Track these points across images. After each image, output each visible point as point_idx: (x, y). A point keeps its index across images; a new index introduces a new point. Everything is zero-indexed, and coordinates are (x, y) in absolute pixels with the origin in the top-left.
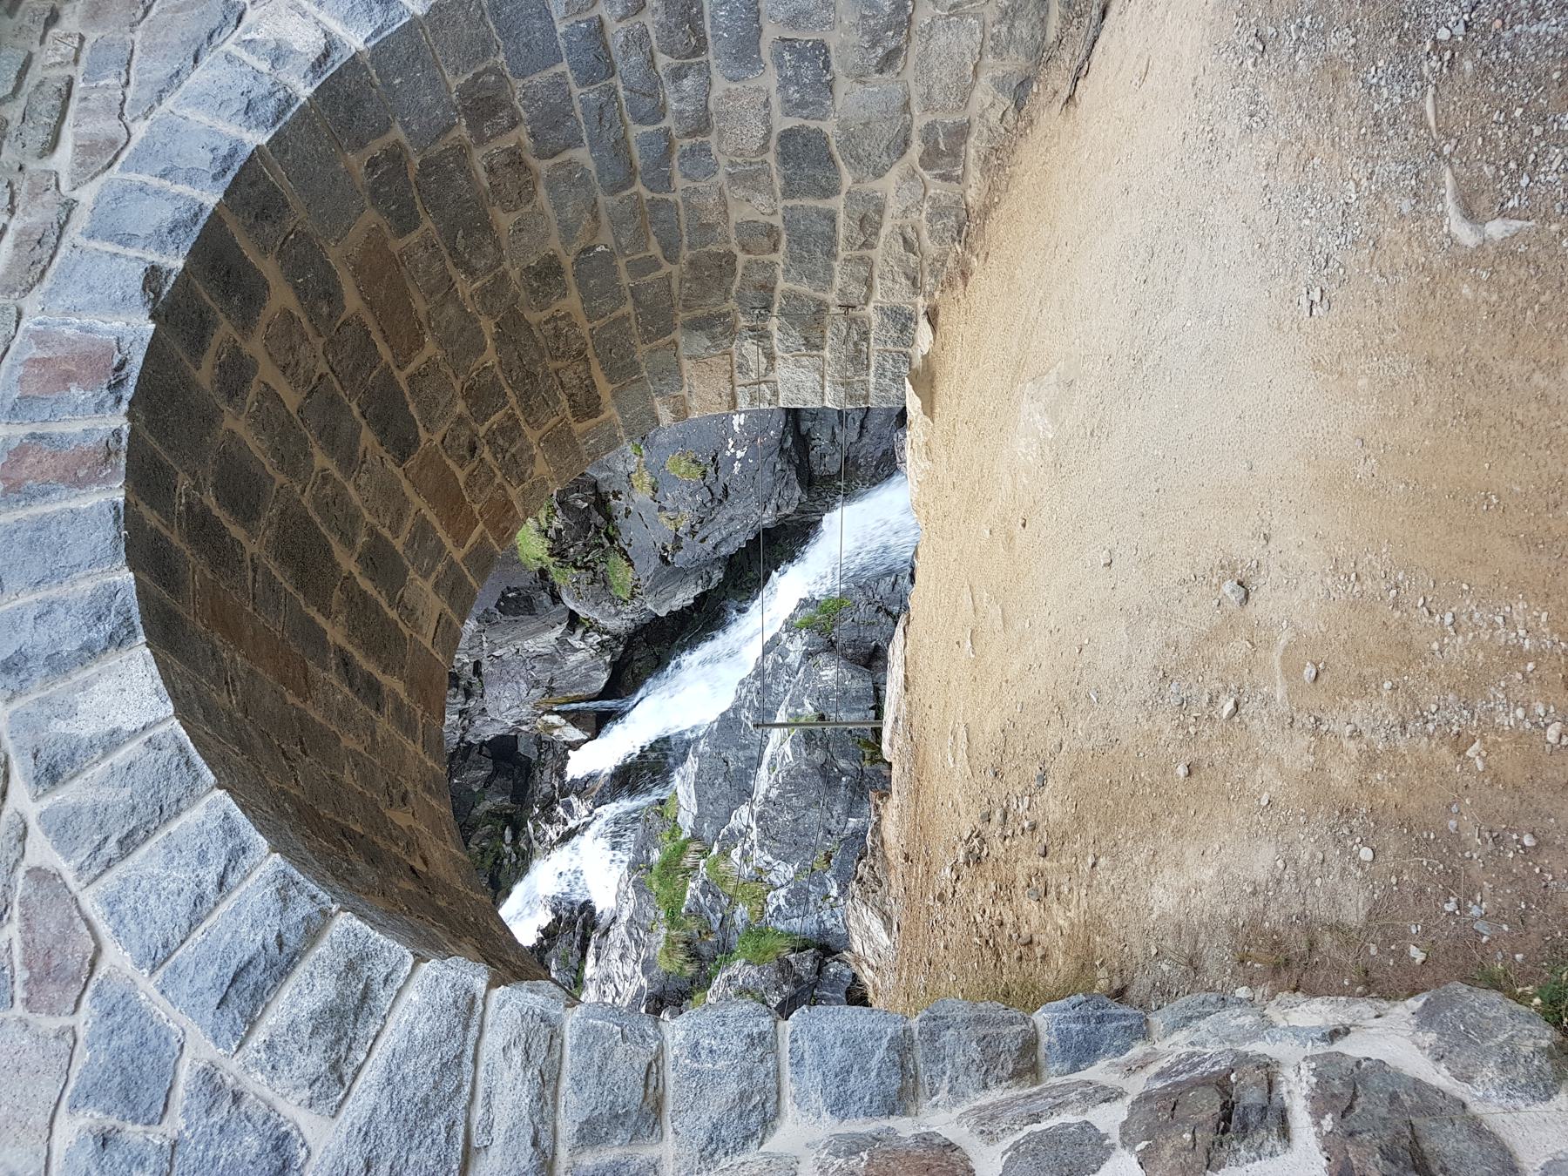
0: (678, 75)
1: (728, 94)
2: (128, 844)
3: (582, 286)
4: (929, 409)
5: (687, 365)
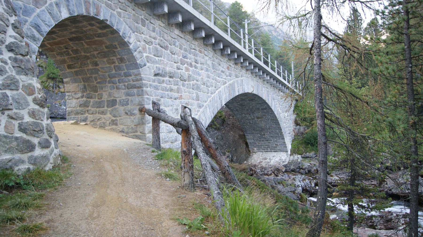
0: (125, 85)
1: (122, 92)
2: (50, 13)
3: (93, 69)
4: (72, 124)
5: (77, 84)
